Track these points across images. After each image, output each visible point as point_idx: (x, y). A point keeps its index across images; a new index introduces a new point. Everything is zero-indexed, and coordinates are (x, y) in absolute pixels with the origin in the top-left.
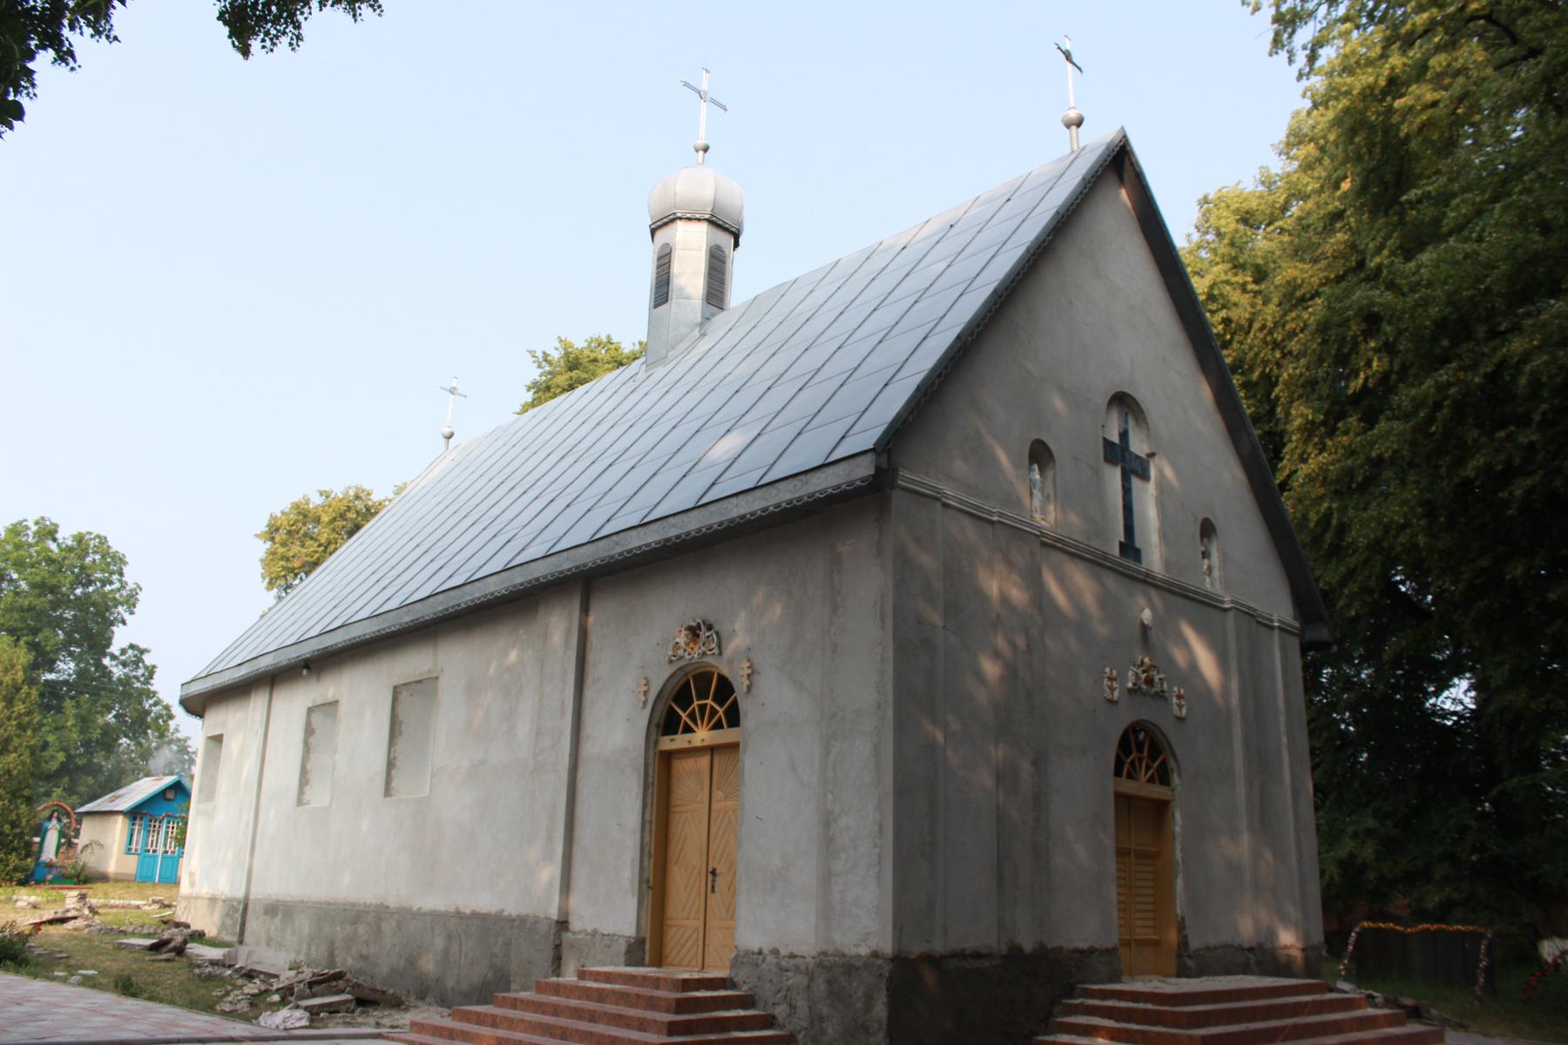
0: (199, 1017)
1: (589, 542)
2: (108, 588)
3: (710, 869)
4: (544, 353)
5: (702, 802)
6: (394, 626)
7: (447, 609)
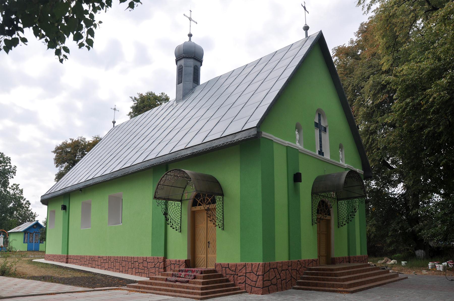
0: (68, 286)
1: (169, 154)
2: (6, 168)
3: (208, 242)
4: (135, 97)
5: (205, 224)
6: (109, 178)
7: (125, 173)
